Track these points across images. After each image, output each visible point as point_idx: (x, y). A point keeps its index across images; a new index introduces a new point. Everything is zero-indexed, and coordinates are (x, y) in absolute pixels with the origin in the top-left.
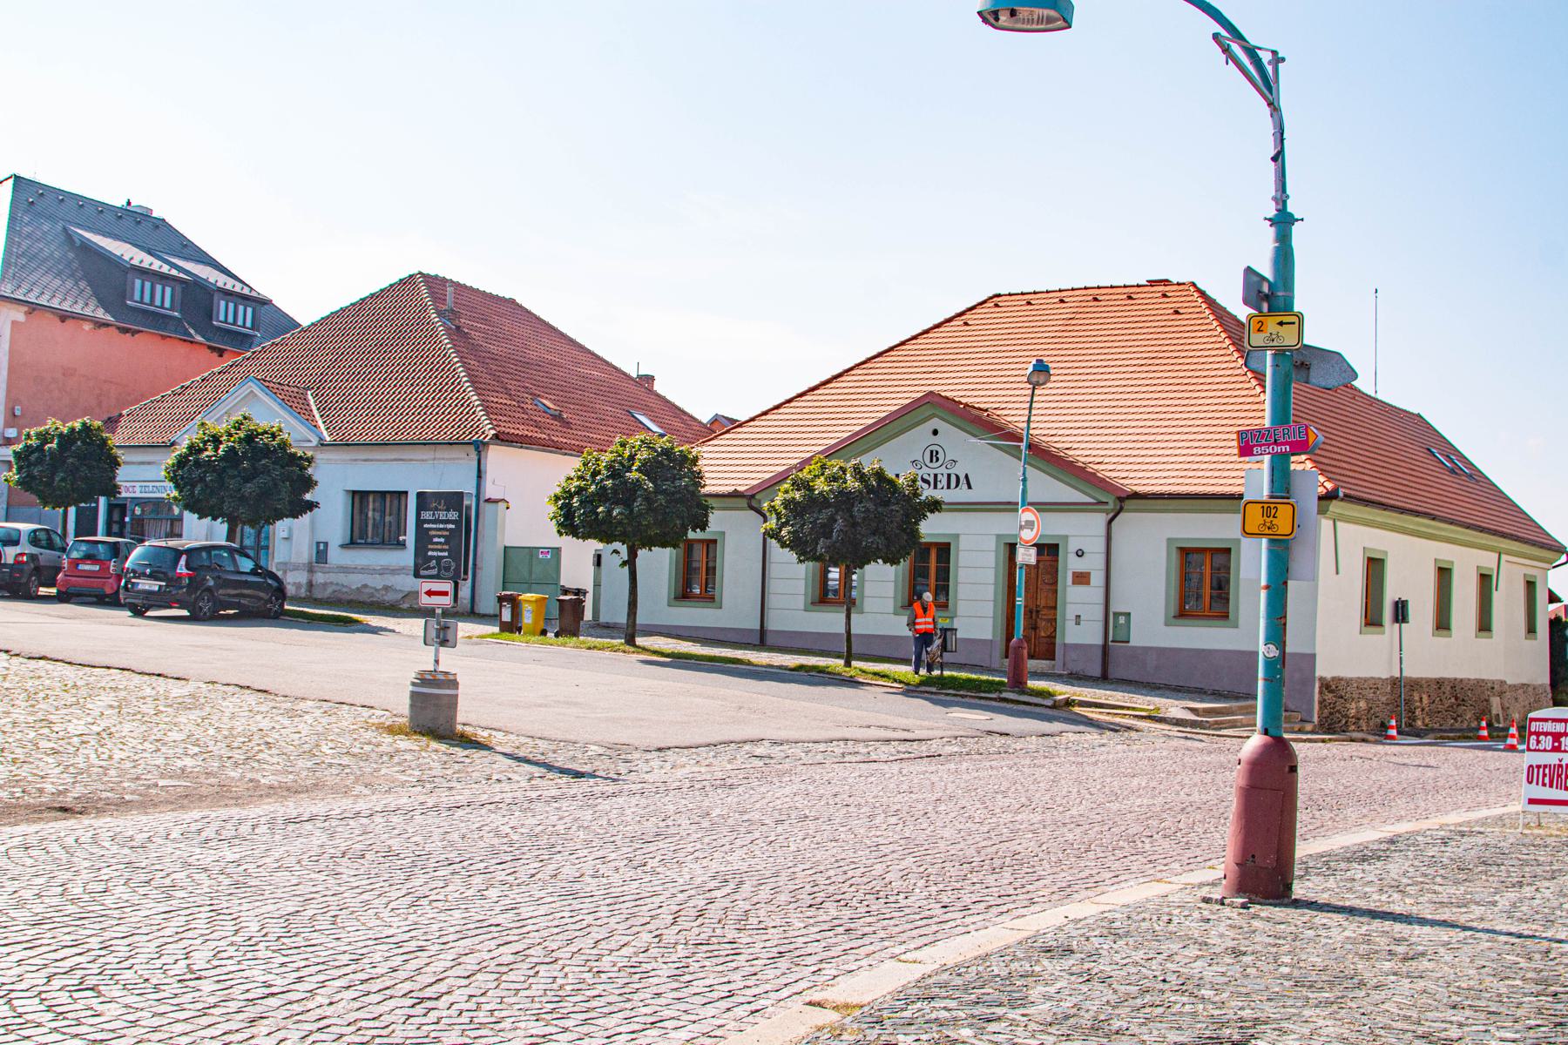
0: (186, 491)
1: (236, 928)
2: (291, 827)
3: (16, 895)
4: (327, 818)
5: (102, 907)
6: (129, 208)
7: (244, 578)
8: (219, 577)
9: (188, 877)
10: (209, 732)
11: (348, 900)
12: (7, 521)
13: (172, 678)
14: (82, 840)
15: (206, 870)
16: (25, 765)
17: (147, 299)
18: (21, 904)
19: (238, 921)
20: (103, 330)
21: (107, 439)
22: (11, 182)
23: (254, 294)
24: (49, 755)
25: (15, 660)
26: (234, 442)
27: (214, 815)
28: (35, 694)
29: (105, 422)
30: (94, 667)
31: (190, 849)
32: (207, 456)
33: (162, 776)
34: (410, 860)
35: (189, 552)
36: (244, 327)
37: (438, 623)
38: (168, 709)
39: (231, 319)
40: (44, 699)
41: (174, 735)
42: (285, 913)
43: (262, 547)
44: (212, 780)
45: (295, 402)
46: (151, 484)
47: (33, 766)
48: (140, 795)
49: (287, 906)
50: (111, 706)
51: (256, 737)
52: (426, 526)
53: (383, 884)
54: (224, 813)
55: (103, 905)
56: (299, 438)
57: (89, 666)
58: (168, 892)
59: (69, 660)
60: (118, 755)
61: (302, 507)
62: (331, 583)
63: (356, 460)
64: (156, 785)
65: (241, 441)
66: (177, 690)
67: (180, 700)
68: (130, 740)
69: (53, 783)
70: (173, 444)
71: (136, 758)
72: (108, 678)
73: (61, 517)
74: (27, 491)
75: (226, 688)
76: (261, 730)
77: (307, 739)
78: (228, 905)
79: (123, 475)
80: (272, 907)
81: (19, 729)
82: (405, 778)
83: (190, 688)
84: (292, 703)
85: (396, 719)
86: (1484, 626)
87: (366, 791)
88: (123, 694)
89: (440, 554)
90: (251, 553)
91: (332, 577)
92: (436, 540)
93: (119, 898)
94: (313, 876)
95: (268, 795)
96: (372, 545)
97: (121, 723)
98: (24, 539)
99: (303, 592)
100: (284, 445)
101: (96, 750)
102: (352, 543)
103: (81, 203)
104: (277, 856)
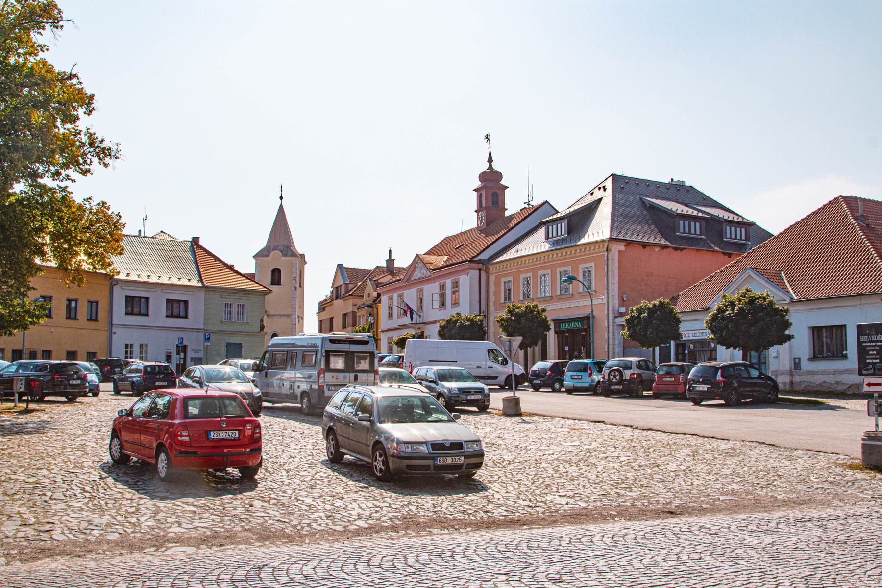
0: (718, 334)
1: (777, 582)
2: (799, 525)
3: (653, 559)
4: (819, 519)
5: (700, 568)
6: (672, 183)
7: (754, 381)
8: (740, 381)
9: (745, 552)
10: (744, 469)
11: (841, 569)
12: (623, 357)
13: (720, 439)
14: (683, 529)
15: (754, 548)
16: (648, 488)
17: (687, 230)
18: (656, 564)
19: (777, 579)
20: (666, 250)
21: (673, 309)
22: (611, 178)
23: (745, 221)
24: (659, 482)
25: (635, 431)
26: (742, 305)
27: (753, 517)
28: (648, 449)
29: (671, 300)
30: (677, 434)
31: (743, 536)
32: (728, 314)
33: (722, 494)
34: (875, 546)
35: (723, 368)
36: (741, 239)
37: (876, 402)
38: (720, 457)
39: (733, 236)
40: (653, 452)
41: (725, 471)
42: (804, 575)
43: (762, 363)
44: (749, 497)
45: (774, 278)
46: (698, 332)
47: (652, 488)
48: (711, 505)
49: (805, 571)
50: (689, 455)
51: (772, 472)
52: (864, 345)
53: (860, 560)
54: (759, 516)
55: (700, 566)
56: (778, 299)
57: (674, 433)
58: (735, 560)
59: (664, 430)
60: (696, 483)
61: (784, 339)
62: (804, 381)
63: (813, 309)
64: (719, 499)
65: (746, 303)
66: (724, 446)
67: (726, 451)
68: (702, 474)
69: (663, 498)
70: (708, 309)
71: (706, 484)
72: (685, 440)
73: (651, 353)
74: (633, 340)
75: (750, 444)
76: (774, 468)
77: (802, 473)
78: (770, 569)
79: (683, 328)
80: (795, 572)
81: (642, 468)
82: (863, 496)
83: (730, 444)
84: (789, 452)
85: (854, 461)
86: (879, 384)
87: (841, 504)
88: (694, 448)
89: (874, 361)
90: (756, 366)
91: (805, 378)
92: (871, 353)
93: (708, 563)
94: (817, 554)
95: (783, 506)
96: (827, 358)
97: (695, 464)
98: (634, 366)
99: (788, 387)
100: (771, 304)
101: (684, 480)
102: (816, 356)
103: (648, 184)
104: (794, 541)
